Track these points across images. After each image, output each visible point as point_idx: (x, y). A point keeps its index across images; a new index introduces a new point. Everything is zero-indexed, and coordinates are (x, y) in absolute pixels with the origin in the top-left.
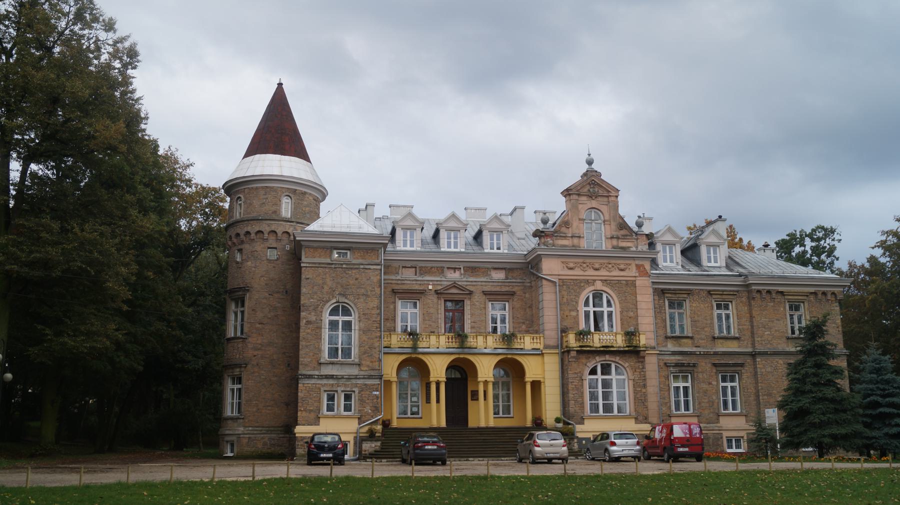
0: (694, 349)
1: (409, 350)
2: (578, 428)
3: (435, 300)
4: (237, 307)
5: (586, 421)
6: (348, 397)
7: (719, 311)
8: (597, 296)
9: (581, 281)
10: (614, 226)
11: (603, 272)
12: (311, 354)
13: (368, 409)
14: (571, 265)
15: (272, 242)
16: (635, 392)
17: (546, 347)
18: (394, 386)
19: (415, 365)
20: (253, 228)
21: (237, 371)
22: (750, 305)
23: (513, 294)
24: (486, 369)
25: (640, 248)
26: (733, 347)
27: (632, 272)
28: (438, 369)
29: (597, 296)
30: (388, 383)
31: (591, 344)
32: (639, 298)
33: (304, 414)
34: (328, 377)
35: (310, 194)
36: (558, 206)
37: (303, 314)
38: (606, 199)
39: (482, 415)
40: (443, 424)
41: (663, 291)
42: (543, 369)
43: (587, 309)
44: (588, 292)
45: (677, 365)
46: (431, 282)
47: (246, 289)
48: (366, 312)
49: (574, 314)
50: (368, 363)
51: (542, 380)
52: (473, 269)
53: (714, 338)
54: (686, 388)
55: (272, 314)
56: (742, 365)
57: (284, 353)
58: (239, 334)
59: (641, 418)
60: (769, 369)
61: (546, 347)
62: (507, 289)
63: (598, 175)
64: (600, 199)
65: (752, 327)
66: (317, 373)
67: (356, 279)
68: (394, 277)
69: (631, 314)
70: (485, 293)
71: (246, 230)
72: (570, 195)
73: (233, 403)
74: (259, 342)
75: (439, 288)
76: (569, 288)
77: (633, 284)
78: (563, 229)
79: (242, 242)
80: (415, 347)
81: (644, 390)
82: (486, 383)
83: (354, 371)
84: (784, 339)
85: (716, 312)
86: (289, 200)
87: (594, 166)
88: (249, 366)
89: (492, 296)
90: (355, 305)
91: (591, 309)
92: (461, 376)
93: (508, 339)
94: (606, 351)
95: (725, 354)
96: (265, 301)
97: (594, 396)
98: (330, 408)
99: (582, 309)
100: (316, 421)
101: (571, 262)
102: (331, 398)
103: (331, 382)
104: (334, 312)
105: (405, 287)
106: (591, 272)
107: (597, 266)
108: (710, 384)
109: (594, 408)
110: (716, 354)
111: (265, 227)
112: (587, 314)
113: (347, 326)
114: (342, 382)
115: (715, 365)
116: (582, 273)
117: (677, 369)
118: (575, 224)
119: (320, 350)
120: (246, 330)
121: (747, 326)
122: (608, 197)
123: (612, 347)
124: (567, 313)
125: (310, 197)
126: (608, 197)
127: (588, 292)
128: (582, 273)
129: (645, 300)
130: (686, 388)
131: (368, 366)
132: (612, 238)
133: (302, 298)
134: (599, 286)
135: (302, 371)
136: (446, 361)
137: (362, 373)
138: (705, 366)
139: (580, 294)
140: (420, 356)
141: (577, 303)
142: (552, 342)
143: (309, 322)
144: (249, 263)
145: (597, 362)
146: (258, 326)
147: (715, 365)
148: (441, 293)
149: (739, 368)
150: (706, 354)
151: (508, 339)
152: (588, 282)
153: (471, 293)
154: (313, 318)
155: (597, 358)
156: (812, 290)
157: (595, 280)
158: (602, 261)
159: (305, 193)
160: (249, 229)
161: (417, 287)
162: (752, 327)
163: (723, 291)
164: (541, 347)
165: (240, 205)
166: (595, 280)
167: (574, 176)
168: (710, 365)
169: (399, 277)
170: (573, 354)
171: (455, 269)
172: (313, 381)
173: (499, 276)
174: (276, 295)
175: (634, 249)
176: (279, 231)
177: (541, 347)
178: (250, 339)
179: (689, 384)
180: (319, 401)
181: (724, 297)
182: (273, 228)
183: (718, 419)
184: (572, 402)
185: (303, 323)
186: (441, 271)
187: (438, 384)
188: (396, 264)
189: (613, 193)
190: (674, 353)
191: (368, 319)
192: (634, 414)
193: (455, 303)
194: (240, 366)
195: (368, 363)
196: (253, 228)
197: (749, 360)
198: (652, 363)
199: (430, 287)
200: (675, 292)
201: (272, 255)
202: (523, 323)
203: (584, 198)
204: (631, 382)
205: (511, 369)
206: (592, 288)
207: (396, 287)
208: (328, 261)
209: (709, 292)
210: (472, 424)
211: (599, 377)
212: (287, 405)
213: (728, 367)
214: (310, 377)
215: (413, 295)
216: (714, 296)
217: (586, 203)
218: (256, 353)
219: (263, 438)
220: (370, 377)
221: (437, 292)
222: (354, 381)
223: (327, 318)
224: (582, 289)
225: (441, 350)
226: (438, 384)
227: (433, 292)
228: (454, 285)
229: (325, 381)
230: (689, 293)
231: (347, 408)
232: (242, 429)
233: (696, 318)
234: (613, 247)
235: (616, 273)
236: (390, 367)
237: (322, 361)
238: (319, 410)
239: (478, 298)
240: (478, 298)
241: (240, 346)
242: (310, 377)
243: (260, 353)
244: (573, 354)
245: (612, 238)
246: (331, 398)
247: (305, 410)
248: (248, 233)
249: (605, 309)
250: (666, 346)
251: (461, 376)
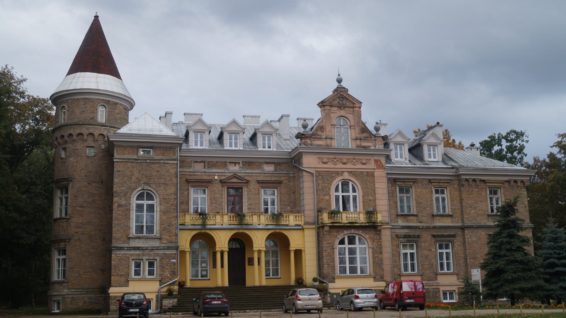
0: (419, 224)
1: (199, 227)
2: (331, 285)
3: (220, 188)
4: (62, 193)
5: (336, 280)
6: (151, 264)
7: (437, 195)
8: (345, 184)
9: (332, 172)
10: (357, 130)
11: (349, 166)
12: (122, 231)
13: (167, 274)
14: (325, 160)
15: (90, 142)
16: (374, 258)
17: (306, 223)
18: (188, 255)
19: (204, 239)
20: (75, 131)
21: (62, 245)
22: (460, 191)
23: (280, 183)
24: (259, 241)
25: (377, 147)
26: (447, 222)
27: (371, 165)
28: (222, 241)
29: (345, 184)
30: (183, 253)
31: (340, 221)
32: (377, 185)
33: (116, 278)
34: (135, 248)
35: (121, 104)
36: (315, 115)
37: (115, 199)
38: (351, 109)
39: (257, 276)
40: (226, 284)
41: (395, 180)
42: (303, 241)
43: (355, 194)
44: (337, 181)
45: (405, 236)
46: (217, 174)
47: (69, 180)
48: (166, 197)
49: (327, 197)
50: (167, 237)
51: (303, 249)
52: (249, 163)
53: (433, 215)
54: (412, 254)
55: (91, 199)
56: (454, 236)
57: (100, 230)
58: (63, 215)
59: (378, 277)
60: (474, 239)
61: (306, 223)
62: (276, 179)
63: (346, 90)
64: (347, 109)
65: (462, 207)
66: (126, 245)
67: (158, 171)
68: (187, 170)
69: (371, 198)
70: (259, 182)
71: (69, 132)
72: (324, 106)
73: (59, 271)
74: (80, 221)
75: (223, 178)
76: (322, 178)
77: (372, 175)
78: (319, 133)
79: (66, 142)
80: (204, 225)
81: (380, 256)
82: (259, 252)
83: (156, 244)
84: (486, 216)
85: (435, 196)
86: (104, 109)
87: (343, 84)
88: (72, 241)
89: (264, 184)
90: (157, 191)
91: (340, 194)
92: (240, 246)
93: (276, 217)
94: (352, 226)
95: (441, 227)
96: (84, 189)
97: (342, 261)
98: (137, 273)
99: (333, 194)
100: (126, 283)
101: (325, 158)
102: (138, 265)
103: (138, 252)
104: (140, 197)
105: (196, 177)
106: (340, 166)
107: (345, 161)
108: (430, 250)
109: (343, 270)
110: (435, 227)
111: (85, 130)
112: (337, 198)
113: (151, 208)
114: (146, 252)
115: (434, 236)
116: (333, 166)
117: (405, 240)
118: (328, 128)
119: (129, 227)
120: (69, 212)
121: (458, 206)
122: (353, 107)
123: (356, 223)
124: (322, 197)
125: (121, 106)
126: (353, 107)
127: (337, 181)
128: (333, 166)
129: (381, 186)
130: (412, 254)
131: (167, 240)
132: (356, 139)
133: (115, 187)
134: (346, 176)
135: (115, 244)
136: (229, 235)
137: (162, 245)
138: (426, 237)
139: (331, 182)
140: (285, 232)
141: (329, 189)
142: (311, 220)
143: (120, 206)
144: (72, 159)
145: (345, 235)
146: (79, 208)
147: (434, 236)
148: (224, 182)
149: (452, 238)
150: (428, 228)
151: (276, 217)
152: (338, 173)
153: (248, 182)
154: (123, 202)
155: (345, 232)
156: (507, 179)
157: (343, 172)
158: (348, 157)
159: (117, 103)
160: (72, 132)
161: (206, 178)
162: (462, 207)
163: (440, 180)
164: (302, 224)
165: (64, 112)
166: (343, 172)
167: (327, 92)
168: (430, 236)
169: (191, 170)
170: (327, 228)
171: (235, 163)
172: (123, 252)
173: (269, 168)
174: (93, 184)
175: (373, 148)
176: (96, 133)
177: (302, 224)
178: (73, 220)
179: (414, 251)
180: (129, 267)
181: (441, 184)
182: (91, 131)
183: (436, 278)
184: (326, 266)
185: (115, 206)
186: (224, 165)
187: (222, 253)
188: (189, 160)
189: (357, 105)
190: (403, 227)
191: (168, 203)
192: (456, 271)
193: (235, 190)
194: (64, 240)
195: (167, 237)
196: (75, 131)
197: (459, 232)
198: (386, 235)
199: (216, 177)
200: (403, 180)
201: (91, 152)
202: (289, 205)
203: (335, 109)
204: (371, 250)
205: (279, 240)
206: (341, 178)
207: (189, 178)
208: (136, 157)
209: (430, 180)
210: (249, 283)
211: (347, 246)
212: (103, 271)
213: (444, 238)
214: (121, 249)
215: (202, 184)
216: (433, 184)
217: (336, 113)
218: (77, 230)
219: (83, 298)
220: (169, 248)
221: (221, 181)
222: (156, 252)
223: (134, 202)
224: (333, 178)
225: (224, 226)
226: (222, 253)
227: (218, 181)
228: (235, 176)
229: (133, 252)
230: (415, 181)
231: (151, 273)
232: (66, 291)
233: (420, 200)
234: (357, 146)
235: (359, 166)
236: (185, 240)
237: (131, 236)
238: (128, 274)
239: (253, 186)
240: (253, 186)
241: (64, 224)
242: (121, 249)
243: (80, 230)
244: (327, 228)
245: (356, 139)
246: (138, 265)
247: (117, 275)
248: (71, 135)
249: (351, 194)
250: (397, 222)
251: (240, 246)
